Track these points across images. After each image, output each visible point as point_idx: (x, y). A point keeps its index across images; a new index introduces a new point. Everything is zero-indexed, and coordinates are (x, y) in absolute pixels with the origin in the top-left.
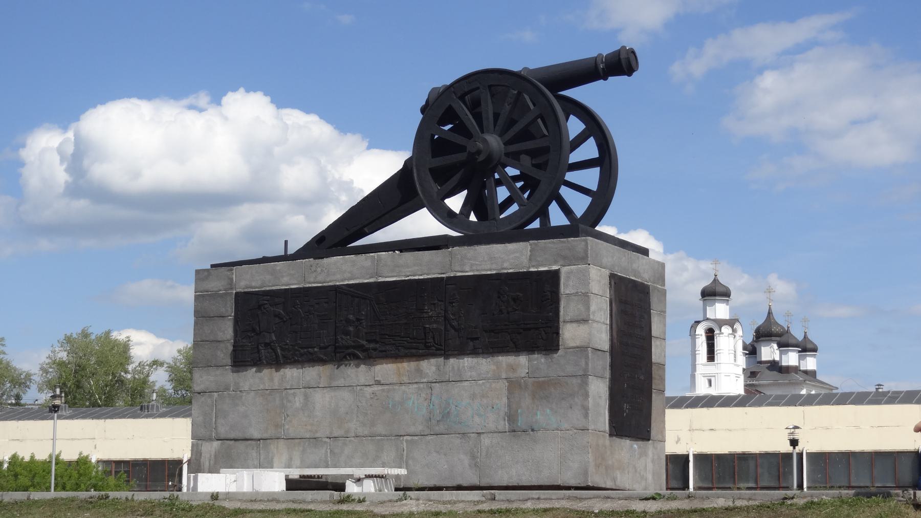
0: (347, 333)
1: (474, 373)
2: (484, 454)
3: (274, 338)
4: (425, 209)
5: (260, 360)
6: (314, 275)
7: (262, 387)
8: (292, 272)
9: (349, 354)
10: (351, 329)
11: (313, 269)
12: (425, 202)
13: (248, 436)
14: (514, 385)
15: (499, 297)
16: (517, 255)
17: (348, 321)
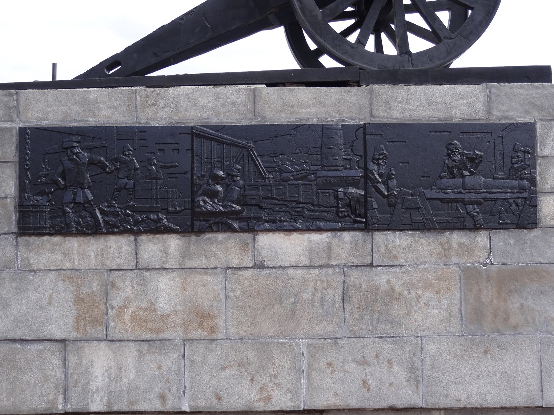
0: (213, 195)
1: (411, 256)
2: (429, 363)
3: (90, 196)
4: (338, 32)
5: (68, 226)
6: (152, 110)
7: (68, 265)
8: (115, 103)
9: (218, 223)
10: (219, 188)
11: (151, 101)
12: (395, 22)
13: (45, 334)
14: (471, 276)
15: (449, 155)
16: (471, 100)
17: (217, 179)
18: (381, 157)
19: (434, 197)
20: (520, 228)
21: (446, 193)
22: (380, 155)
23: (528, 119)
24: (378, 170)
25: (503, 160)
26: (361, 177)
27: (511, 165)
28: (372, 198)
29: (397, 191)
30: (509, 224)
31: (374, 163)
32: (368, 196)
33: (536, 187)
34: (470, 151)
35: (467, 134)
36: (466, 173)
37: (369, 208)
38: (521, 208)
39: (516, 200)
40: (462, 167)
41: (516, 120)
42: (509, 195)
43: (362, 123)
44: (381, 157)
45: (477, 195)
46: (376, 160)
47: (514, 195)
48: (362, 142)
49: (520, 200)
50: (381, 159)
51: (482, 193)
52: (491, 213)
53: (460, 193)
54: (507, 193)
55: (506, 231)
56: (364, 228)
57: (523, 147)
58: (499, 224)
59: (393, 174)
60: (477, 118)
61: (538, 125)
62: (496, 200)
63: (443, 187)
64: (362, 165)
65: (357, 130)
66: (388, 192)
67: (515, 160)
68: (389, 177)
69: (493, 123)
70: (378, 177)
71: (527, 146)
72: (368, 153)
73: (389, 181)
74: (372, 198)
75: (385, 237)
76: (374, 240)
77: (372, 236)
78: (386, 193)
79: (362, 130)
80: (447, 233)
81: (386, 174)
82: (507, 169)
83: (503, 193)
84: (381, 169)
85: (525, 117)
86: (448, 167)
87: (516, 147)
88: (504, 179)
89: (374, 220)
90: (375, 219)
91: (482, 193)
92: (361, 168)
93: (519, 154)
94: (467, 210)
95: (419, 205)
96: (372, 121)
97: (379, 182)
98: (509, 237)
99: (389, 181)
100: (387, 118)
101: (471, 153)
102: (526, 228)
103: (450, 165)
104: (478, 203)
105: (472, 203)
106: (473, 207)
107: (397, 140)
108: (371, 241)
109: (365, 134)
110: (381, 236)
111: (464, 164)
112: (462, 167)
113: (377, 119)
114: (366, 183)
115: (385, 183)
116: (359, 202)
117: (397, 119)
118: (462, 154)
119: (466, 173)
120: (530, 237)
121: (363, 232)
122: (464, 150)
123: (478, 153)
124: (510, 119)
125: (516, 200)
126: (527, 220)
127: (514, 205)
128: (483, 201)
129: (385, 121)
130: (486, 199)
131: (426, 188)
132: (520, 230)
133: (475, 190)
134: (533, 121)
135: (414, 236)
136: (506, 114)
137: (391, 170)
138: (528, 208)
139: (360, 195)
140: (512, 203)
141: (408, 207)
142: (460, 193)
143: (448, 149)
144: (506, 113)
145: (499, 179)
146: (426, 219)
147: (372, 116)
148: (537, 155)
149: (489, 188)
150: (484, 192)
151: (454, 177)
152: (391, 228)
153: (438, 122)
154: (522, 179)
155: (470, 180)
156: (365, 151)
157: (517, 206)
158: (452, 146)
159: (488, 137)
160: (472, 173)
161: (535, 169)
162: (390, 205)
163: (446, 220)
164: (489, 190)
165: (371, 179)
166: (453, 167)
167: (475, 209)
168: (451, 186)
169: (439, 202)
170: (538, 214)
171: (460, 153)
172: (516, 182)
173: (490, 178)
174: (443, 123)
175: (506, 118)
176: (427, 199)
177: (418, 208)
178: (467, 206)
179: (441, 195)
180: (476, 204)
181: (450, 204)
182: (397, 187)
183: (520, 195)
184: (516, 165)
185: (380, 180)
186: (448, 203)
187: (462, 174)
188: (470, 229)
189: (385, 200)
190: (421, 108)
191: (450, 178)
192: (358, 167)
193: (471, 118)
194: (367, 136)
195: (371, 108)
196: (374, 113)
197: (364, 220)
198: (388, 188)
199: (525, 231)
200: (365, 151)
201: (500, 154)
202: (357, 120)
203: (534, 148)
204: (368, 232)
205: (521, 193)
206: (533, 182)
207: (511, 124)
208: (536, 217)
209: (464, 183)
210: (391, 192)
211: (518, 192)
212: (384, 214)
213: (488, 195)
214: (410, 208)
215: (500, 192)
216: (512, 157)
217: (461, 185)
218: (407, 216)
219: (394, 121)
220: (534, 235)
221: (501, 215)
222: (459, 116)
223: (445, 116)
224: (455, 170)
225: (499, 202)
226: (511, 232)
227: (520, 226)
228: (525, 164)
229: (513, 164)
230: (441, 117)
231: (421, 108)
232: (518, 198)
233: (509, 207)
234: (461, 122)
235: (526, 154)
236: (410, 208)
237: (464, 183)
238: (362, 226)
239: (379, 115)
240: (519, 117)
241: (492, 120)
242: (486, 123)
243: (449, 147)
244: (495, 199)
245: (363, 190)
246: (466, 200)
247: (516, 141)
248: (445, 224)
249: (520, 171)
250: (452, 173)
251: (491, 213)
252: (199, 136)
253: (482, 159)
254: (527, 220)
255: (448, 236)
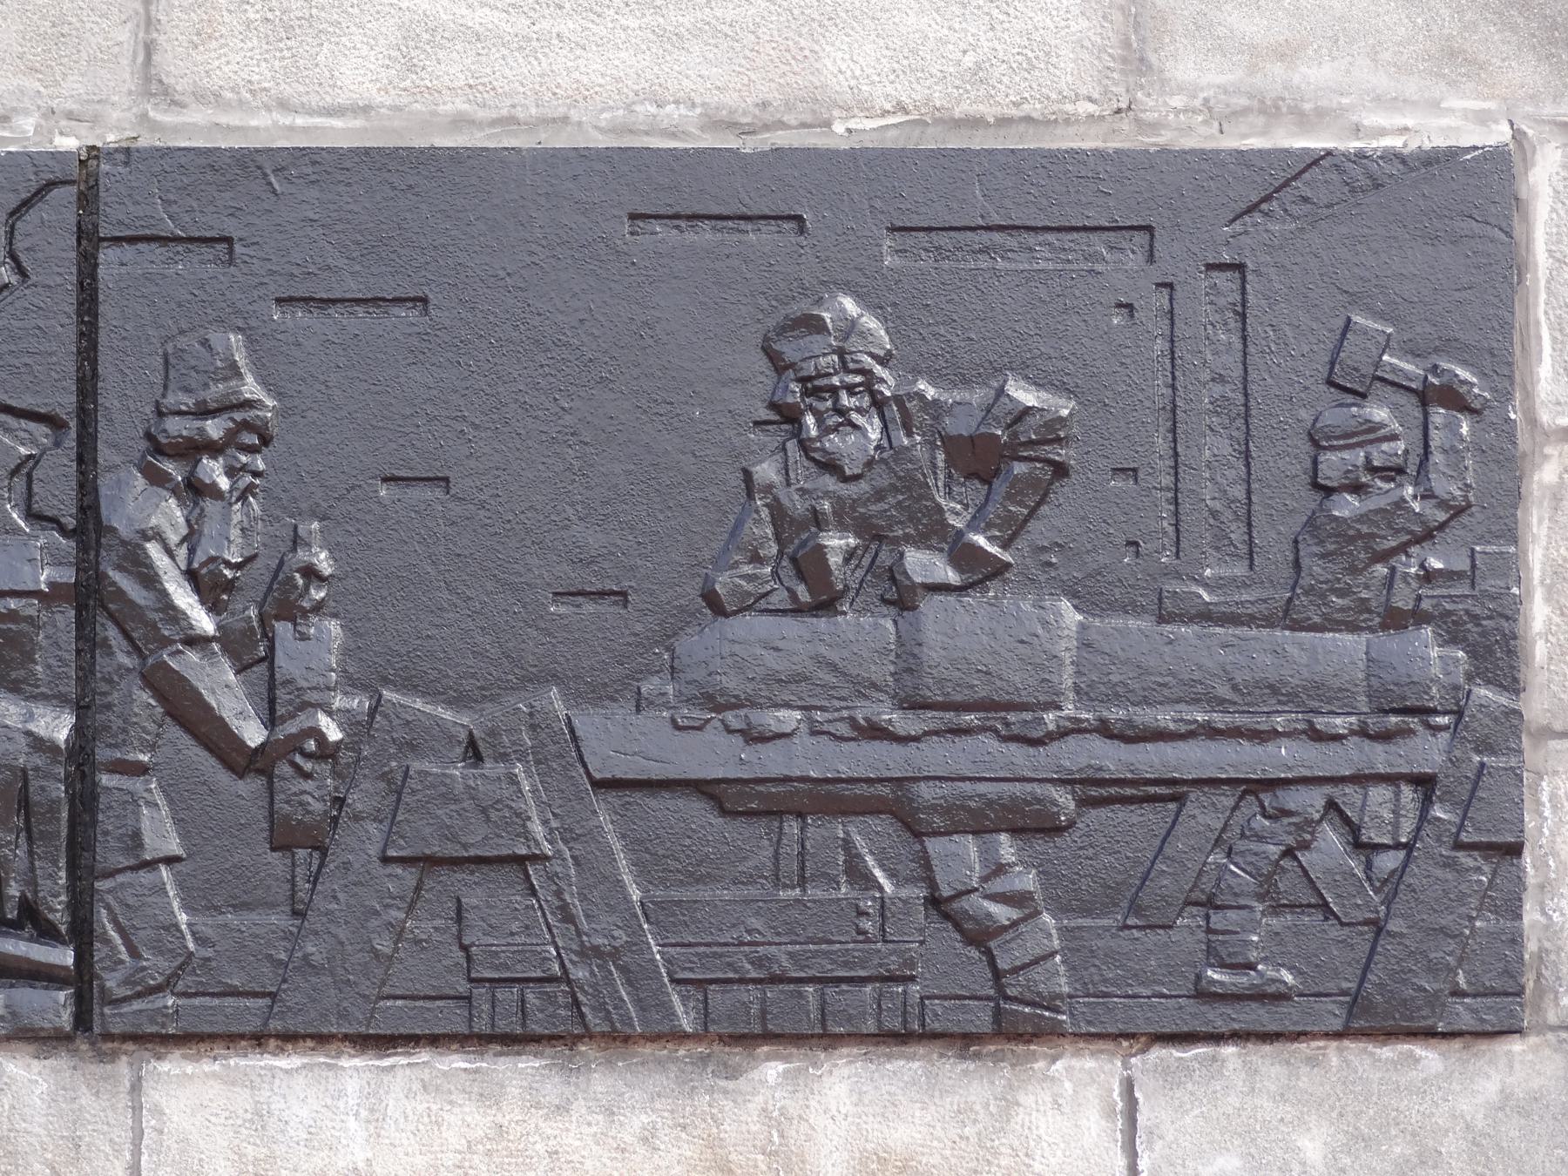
18: (214, 429)
19: (656, 772)
20: (1389, 1035)
21: (755, 737)
22: (204, 412)
23: (1454, 121)
24: (192, 538)
25: (1247, 455)
26: (52, 596)
27: (1311, 500)
28: (141, 770)
29: (346, 719)
30: (1281, 997)
31: (156, 478)
32: (103, 754)
33: (1512, 684)
34: (966, 382)
35: (943, 239)
36: (925, 564)
37: (109, 854)
38: (1388, 862)
39: (1349, 796)
40: (893, 514)
41: (1357, 130)
42: (1285, 756)
43: (68, 143)
44: (214, 429)
45: (1018, 754)
46: (172, 457)
47: (1332, 748)
48: (67, 303)
49: (1379, 795)
50: (214, 449)
51: (1062, 734)
52: (1143, 912)
53: (875, 732)
54: (1274, 734)
55: (1261, 1054)
56: (66, 1019)
57: (1415, 354)
58: (1204, 994)
59: (310, 573)
60: (1034, 108)
61: (1542, 178)
62: (1180, 799)
63: (732, 683)
64: (59, 496)
65: (26, 204)
66: (271, 721)
67: (1333, 464)
68: (285, 604)
69: (1164, 151)
70: (184, 598)
71: (1448, 346)
72: (109, 398)
73: (283, 629)
74: (141, 770)
75: (242, 1100)
76: (149, 1122)
77: (136, 1088)
78: (254, 734)
79: (61, 208)
80: (773, 1070)
81: (261, 571)
82: (1274, 539)
83: (1235, 733)
84: (210, 528)
85: (1434, 106)
86: (778, 513)
87: (1353, 351)
88: (1250, 621)
89: (149, 958)
90: (159, 951)
91: (1062, 734)
92: (55, 522)
93: (1380, 414)
94: (932, 884)
95: (527, 835)
96: (155, 127)
97: (196, 641)
98: (1288, 1112)
99: (283, 629)
100: (284, 105)
101: (977, 396)
102: (1428, 1034)
103: (798, 506)
104: (1034, 825)
105: (979, 822)
106: (987, 853)
107: (353, 289)
108: (124, 1136)
109: (88, 240)
110: (216, 1088)
111: (912, 487)
112: (893, 514)
113: (197, 116)
114: (88, 643)
115: (248, 650)
116: (25, 804)
117: (366, 110)
118: (896, 411)
119: (925, 564)
120: (1464, 1106)
121: (61, 1062)
122: (917, 372)
123: (1027, 397)
124: (1304, 120)
125: (1349, 796)
126: (1433, 969)
127: (1331, 838)
128: (1064, 800)
129: (265, 128)
130: (1096, 791)
131: (595, 693)
132: (1387, 1052)
133: (1000, 712)
134: (1500, 134)
135: (489, 1097)
136: (1275, 77)
137: (296, 541)
138: (1450, 864)
139: (39, 744)
140: (1310, 824)
141: (436, 849)
142: (875, 732)
143: (773, 357)
144: (1277, 69)
145: (1206, 616)
146: (589, 953)
147: (152, 85)
148: (1533, 422)
149: (1116, 696)
150: (1076, 729)
151: (826, 604)
152: (293, 1024)
153: (708, 141)
154: (1395, 620)
155: (957, 633)
156: (87, 386)
157: (1359, 846)
158: (816, 343)
159: (1124, 266)
160: (979, 572)
161: (1511, 533)
162: (284, 836)
163: (758, 963)
164: (1116, 714)
165: (126, 617)
166: (817, 520)
167: (1000, 869)
168: (798, 678)
169: (696, 810)
170: (1531, 915)
171: (879, 404)
172: (1350, 646)
173: (1129, 608)
174: (749, 145)
175: (1270, 110)
176: (598, 785)
177: (520, 861)
178: (934, 846)
179: (714, 754)
180: (1015, 831)
181: (792, 827)
182: (352, 683)
183: (1380, 758)
184: (1347, 506)
185: (205, 623)
186: (779, 814)
187: (895, 575)
188: (964, 1042)
189: (250, 787)
190: (567, 26)
191: (798, 610)
192: (32, 515)
193: (982, 109)
194: (108, 256)
195: (149, 23)
196: (174, 64)
197: (66, 957)
198: (272, 685)
199: (1429, 1057)
200: (87, 386)
201: (1219, 405)
202: (28, 124)
203: (1502, 356)
204: (102, 1057)
205: (1385, 736)
206: (1495, 649)
207: (1316, 160)
208: (1516, 941)
209: (908, 657)
210: (291, 728)
211: (1363, 732)
212: (240, 906)
213: (1111, 758)
214: (455, 862)
215: (1212, 732)
216: (1317, 441)
217: (882, 671)
218: (422, 927)
219: (341, 133)
220: (1506, 1095)
221: (1217, 920)
222: (883, 93)
223: (767, 91)
224: (836, 543)
225: (1204, 814)
226: (1312, 1061)
227: (1378, 1017)
228: (1428, 495)
229: (1328, 491)
230: (730, 99)
231: (567, 26)
232: (1362, 779)
233: (1289, 853)
234: (892, 141)
235: (1439, 415)
236: (455, 862)
237: (908, 657)
238: (57, 1006)
239: (215, 82)
240: (1381, 101)
241: (1154, 127)
242: (1099, 154)
243: (789, 349)
244: (1172, 791)
245: (60, 700)
246: (926, 792)
247: (1354, 299)
248: (750, 994)
249: (1384, 557)
250: (810, 566)
251: (1135, 908)
252: (272, 710)
253: (1060, 454)
254: (1433, 969)
255: (782, 1098)
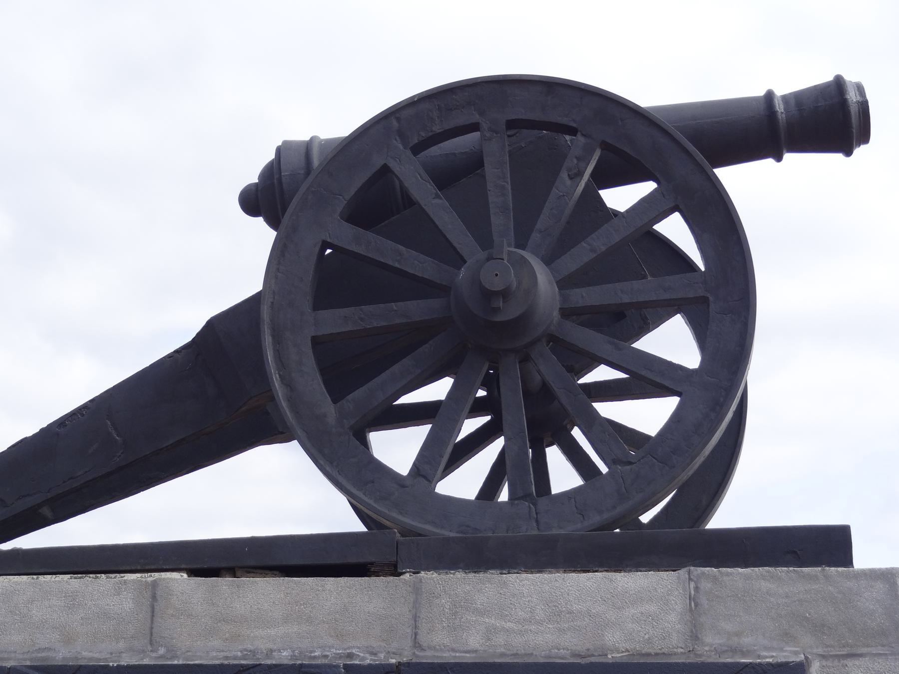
16: (652, 608)
129: (448, 657)
147: (417, 645)
196: (423, 639)
219: (468, 658)
222: (623, 646)
